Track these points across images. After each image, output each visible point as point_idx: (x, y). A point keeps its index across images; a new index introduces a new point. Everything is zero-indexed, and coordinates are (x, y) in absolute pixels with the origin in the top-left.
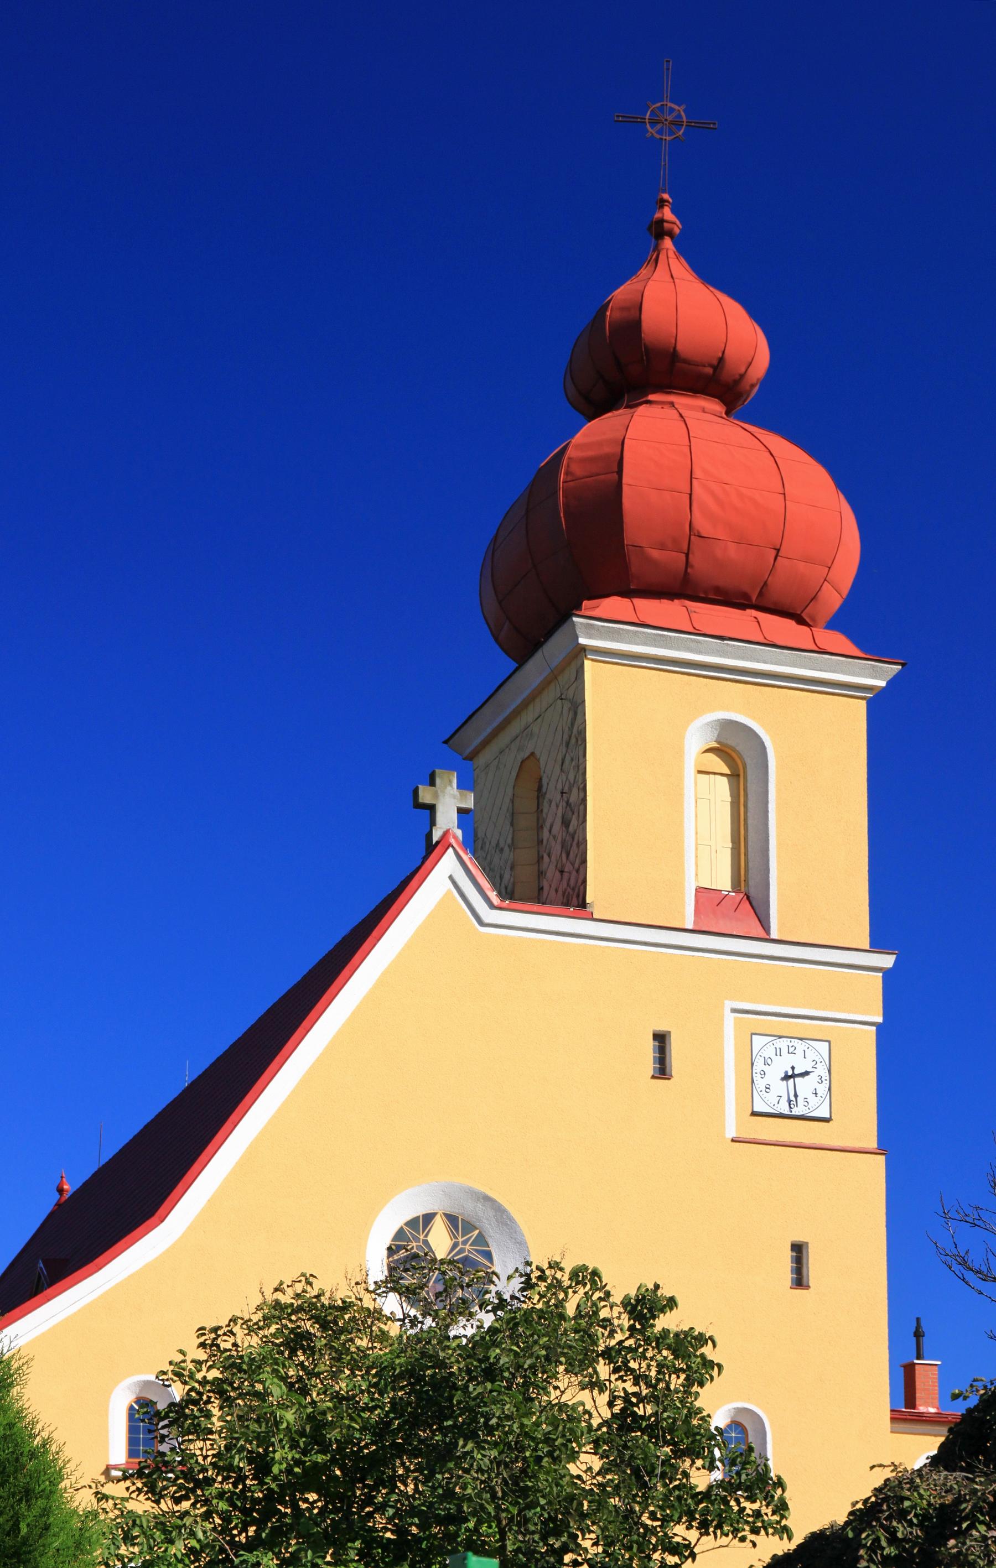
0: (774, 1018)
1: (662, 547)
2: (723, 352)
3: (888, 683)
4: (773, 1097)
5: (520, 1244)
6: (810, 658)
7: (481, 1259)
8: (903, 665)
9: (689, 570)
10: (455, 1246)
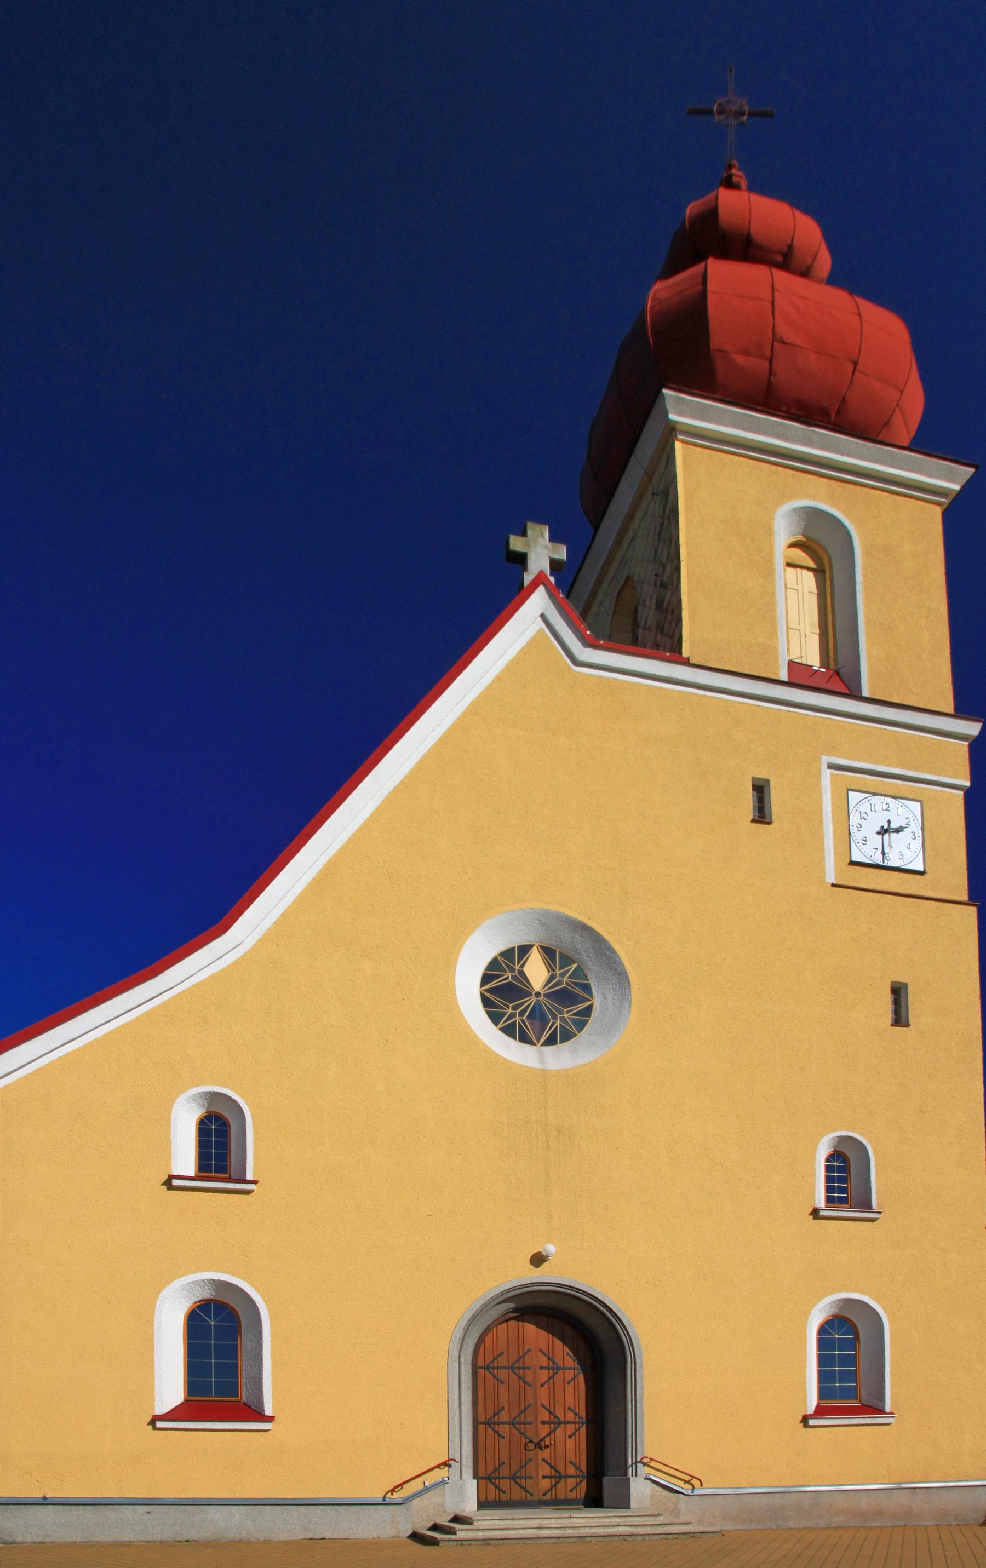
0: (868, 777)
1: (746, 352)
3: (963, 488)
4: (865, 852)
5: (620, 974)
7: (579, 992)
8: (976, 467)
9: (772, 379)
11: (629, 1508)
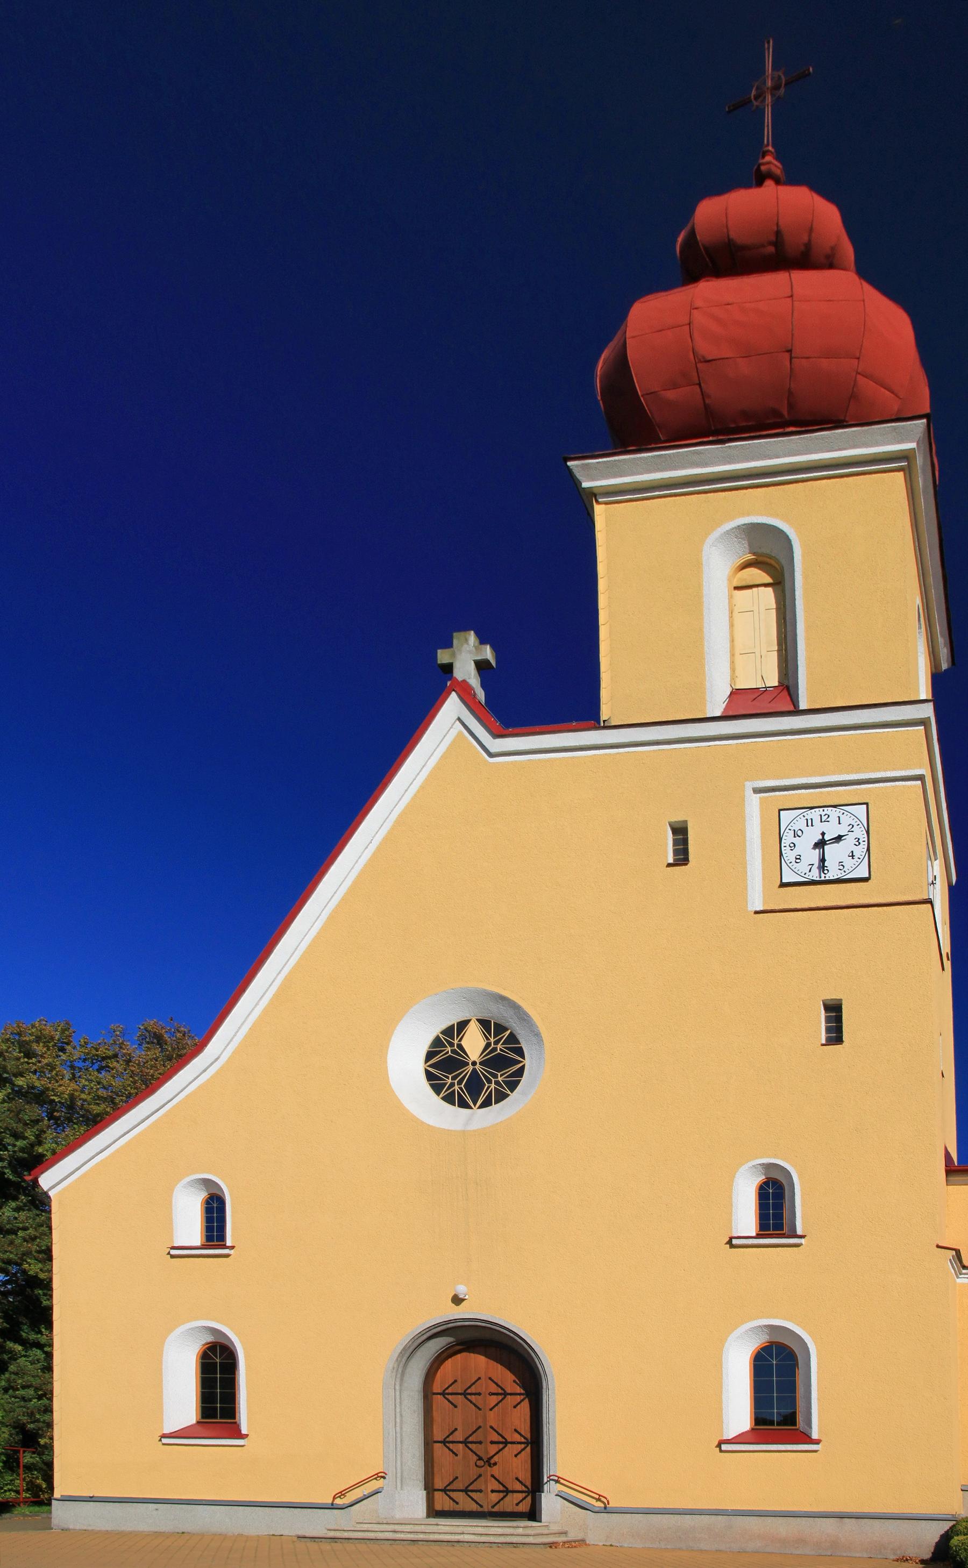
1: (675, 386)
2: (777, 224)
4: (804, 863)
6: (822, 438)
10: (488, 1045)
11: (540, 1521)
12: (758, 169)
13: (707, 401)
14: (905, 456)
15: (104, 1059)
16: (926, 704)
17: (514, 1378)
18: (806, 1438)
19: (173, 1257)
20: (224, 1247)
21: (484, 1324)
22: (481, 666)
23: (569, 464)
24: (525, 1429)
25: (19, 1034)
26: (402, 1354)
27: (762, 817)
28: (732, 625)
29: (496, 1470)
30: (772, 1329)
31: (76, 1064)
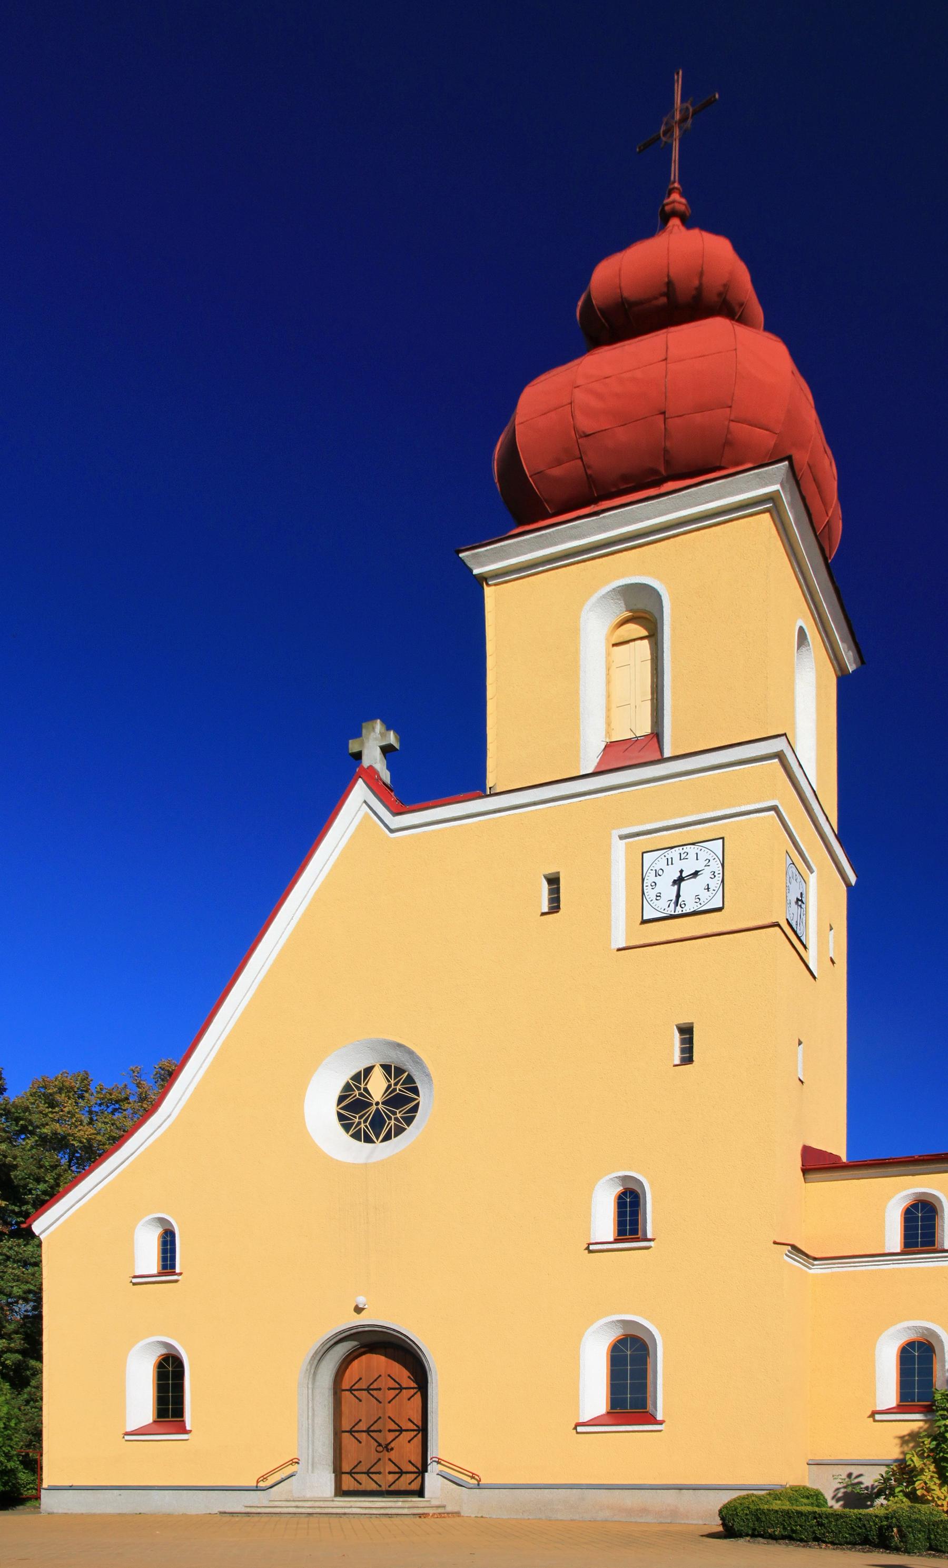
0: (665, 833)
1: (559, 462)
2: (668, 276)
6: (689, 495)
10: (389, 1086)
12: (663, 209)
13: (589, 472)
14: (772, 498)
15: (117, 1102)
16: (779, 739)
17: (409, 1374)
18: (651, 1419)
19: (134, 1284)
20: (174, 1273)
21: (348, 1333)
22: (387, 750)
23: (461, 555)
24: (418, 1420)
25: (45, 1087)
26: (313, 1357)
27: (627, 859)
28: (608, 682)
29: (393, 1455)
30: (625, 1323)
31: (93, 1109)
